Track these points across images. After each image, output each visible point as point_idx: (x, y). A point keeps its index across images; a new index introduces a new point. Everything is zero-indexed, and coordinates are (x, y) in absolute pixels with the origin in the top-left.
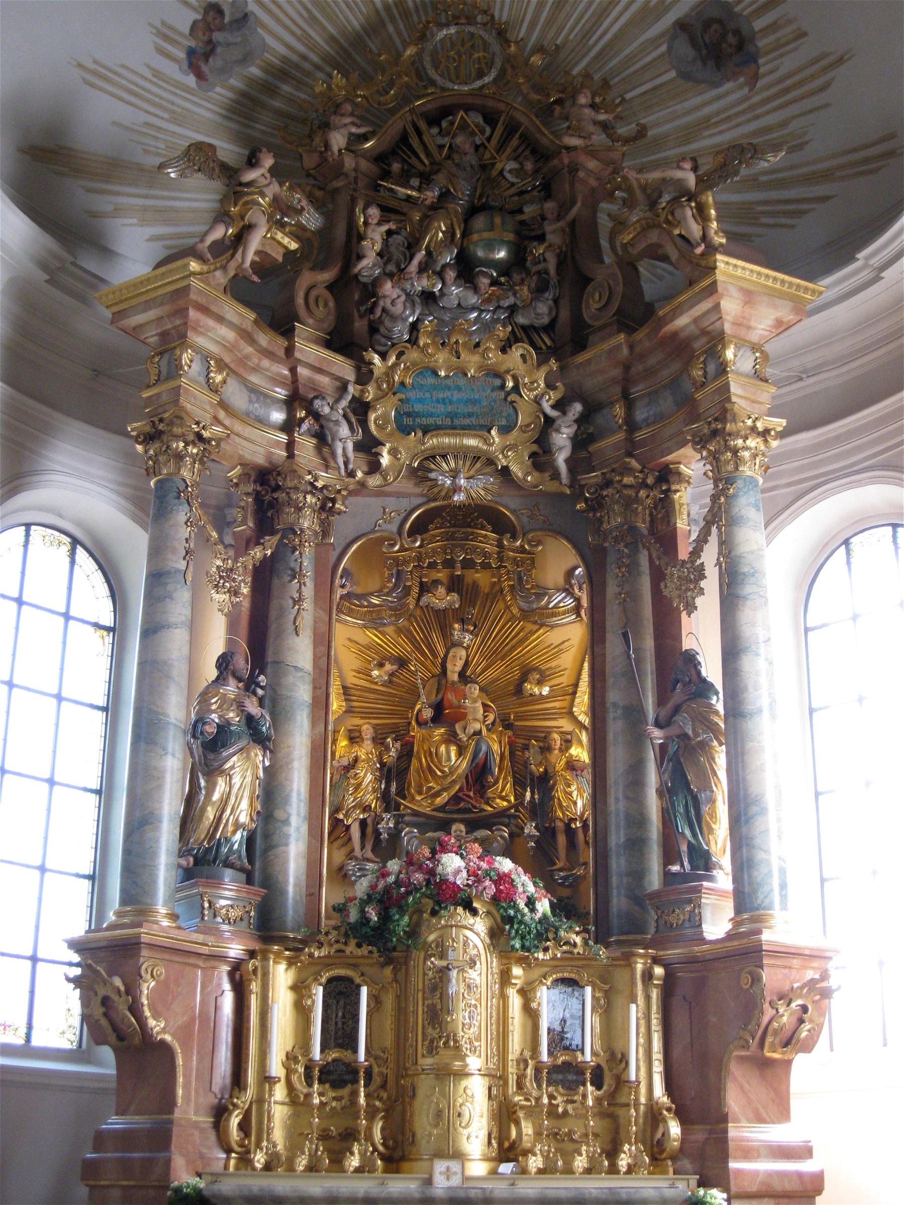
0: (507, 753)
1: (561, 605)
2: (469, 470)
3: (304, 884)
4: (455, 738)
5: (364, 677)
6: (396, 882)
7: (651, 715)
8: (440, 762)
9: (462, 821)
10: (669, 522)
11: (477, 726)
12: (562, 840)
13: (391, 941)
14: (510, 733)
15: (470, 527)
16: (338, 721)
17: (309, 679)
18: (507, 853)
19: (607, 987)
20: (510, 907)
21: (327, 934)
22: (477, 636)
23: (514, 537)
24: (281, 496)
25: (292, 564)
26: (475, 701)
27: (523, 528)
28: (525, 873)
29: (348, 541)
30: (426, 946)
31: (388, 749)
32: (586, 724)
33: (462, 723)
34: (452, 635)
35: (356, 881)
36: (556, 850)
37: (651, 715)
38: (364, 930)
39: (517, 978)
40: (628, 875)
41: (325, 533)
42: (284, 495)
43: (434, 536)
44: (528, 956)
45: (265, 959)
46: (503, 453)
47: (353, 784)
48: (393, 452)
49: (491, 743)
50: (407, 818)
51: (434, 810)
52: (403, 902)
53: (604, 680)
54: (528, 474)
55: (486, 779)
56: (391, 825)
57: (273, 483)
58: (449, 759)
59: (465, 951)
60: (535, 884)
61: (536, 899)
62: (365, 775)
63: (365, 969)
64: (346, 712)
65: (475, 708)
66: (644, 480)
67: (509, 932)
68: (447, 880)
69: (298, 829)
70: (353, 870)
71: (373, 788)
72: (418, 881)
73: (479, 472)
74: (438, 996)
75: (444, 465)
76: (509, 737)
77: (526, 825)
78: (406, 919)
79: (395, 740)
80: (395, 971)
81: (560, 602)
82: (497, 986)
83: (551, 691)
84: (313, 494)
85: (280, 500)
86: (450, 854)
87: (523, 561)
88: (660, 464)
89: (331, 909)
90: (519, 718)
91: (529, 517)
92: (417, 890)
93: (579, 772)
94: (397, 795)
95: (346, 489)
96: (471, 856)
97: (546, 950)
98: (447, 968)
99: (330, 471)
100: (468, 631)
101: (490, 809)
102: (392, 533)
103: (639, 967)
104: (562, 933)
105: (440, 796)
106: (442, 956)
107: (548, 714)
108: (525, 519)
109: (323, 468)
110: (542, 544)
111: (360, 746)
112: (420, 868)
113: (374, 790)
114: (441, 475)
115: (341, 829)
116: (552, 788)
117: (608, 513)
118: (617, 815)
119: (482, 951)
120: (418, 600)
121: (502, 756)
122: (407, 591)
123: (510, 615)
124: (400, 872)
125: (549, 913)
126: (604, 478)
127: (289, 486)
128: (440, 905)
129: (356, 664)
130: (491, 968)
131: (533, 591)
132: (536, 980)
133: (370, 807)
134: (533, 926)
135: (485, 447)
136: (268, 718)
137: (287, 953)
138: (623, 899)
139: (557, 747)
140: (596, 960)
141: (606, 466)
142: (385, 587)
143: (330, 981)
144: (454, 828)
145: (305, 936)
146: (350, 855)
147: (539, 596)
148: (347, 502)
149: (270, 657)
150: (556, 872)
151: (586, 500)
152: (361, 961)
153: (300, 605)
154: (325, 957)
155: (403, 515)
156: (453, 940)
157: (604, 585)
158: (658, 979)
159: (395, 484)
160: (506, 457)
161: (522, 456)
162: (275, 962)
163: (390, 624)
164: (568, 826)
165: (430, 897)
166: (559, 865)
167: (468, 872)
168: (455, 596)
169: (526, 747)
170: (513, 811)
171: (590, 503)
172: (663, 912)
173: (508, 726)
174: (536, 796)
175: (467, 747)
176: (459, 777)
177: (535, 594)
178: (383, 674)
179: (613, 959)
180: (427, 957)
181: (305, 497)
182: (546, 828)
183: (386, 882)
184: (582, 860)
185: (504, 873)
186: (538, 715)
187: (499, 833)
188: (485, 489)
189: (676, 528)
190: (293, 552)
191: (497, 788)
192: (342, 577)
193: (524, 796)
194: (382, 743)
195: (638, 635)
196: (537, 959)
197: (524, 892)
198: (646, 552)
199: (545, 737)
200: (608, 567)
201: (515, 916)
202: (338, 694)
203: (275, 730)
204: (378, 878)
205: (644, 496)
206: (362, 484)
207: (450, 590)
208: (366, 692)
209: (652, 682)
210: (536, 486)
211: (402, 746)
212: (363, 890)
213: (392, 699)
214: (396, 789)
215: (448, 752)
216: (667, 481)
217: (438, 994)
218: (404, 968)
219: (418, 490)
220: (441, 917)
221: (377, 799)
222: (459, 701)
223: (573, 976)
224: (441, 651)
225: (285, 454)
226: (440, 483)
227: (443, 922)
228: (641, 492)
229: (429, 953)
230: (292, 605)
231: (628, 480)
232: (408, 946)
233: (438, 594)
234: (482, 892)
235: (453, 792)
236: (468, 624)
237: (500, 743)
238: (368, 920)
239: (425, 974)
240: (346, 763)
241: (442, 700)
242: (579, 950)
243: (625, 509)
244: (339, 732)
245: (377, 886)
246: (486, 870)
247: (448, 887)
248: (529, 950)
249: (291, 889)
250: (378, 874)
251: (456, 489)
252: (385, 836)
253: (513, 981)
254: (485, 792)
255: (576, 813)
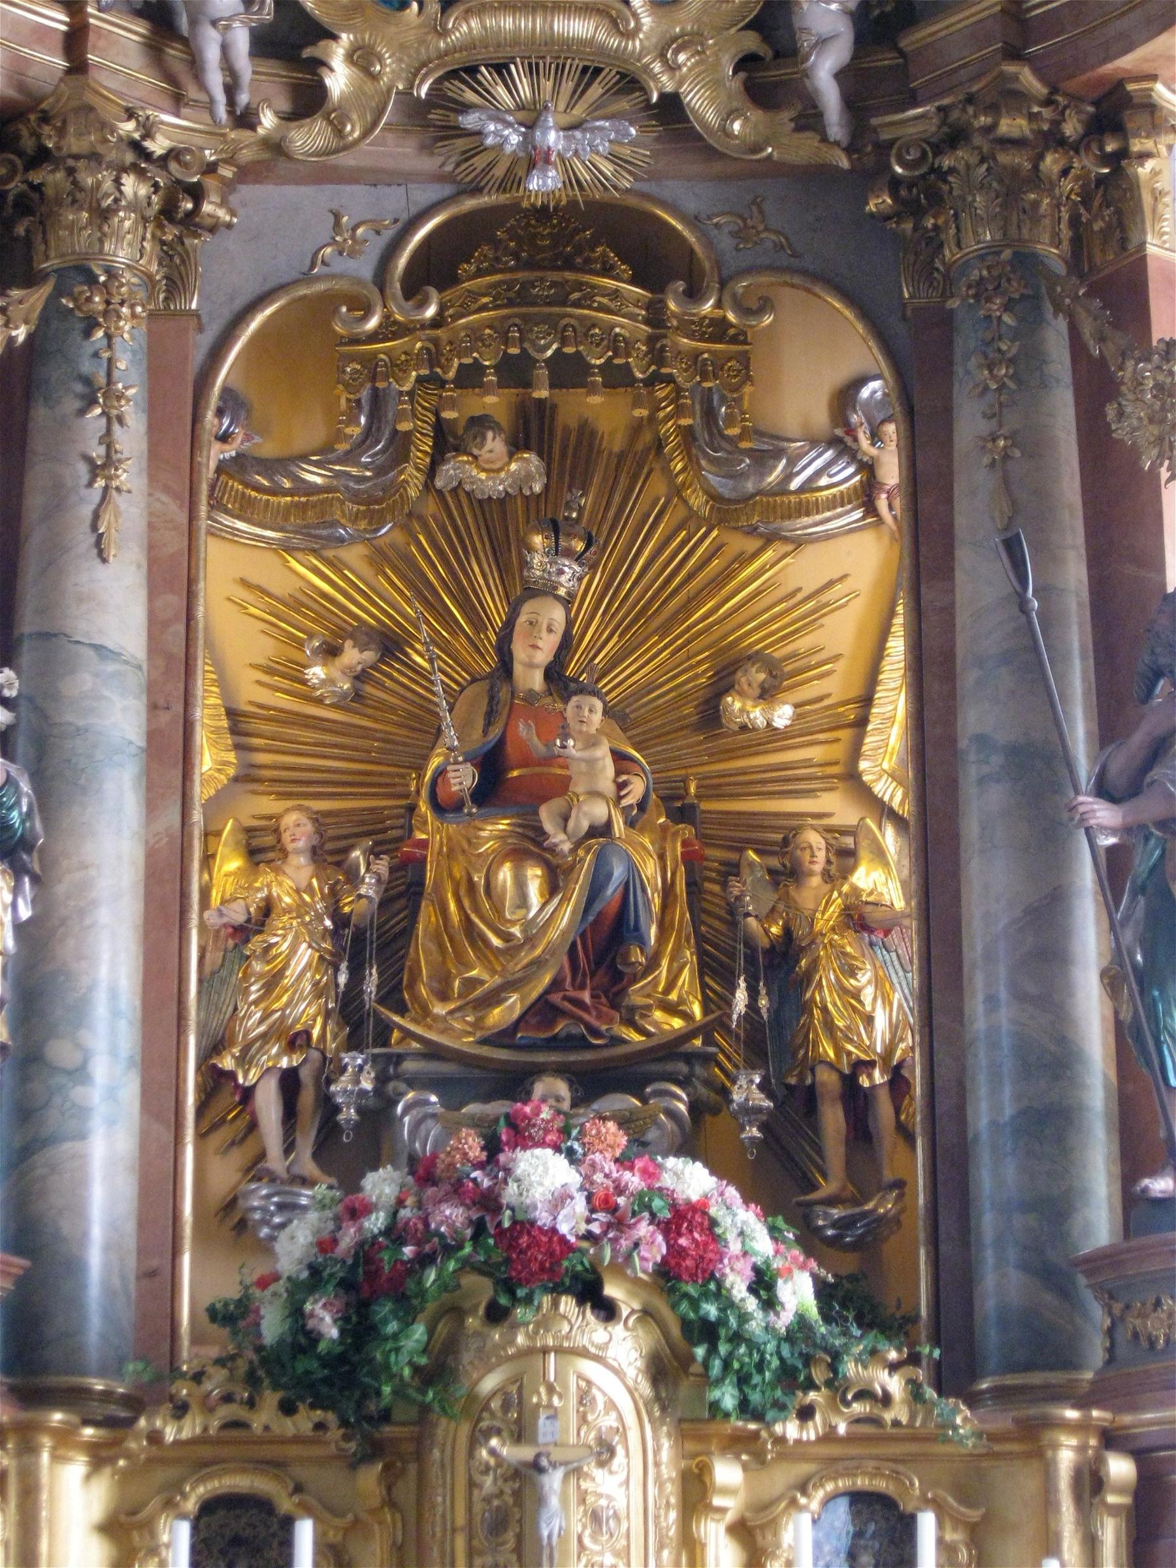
0: (681, 886)
1: (824, 481)
2: (570, 106)
3: (131, 1243)
4: (539, 844)
5: (286, 684)
6: (388, 1231)
7: (1084, 768)
8: (499, 910)
9: (560, 1070)
10: (1124, 242)
11: (599, 811)
12: (833, 1119)
13: (378, 1393)
14: (687, 831)
15: (569, 265)
16: (215, 805)
17: (136, 680)
18: (688, 1148)
19: (974, 1515)
20: (706, 1295)
21: (198, 1377)
22: (593, 567)
23: (694, 294)
24: (52, 178)
25: (86, 367)
26: (591, 742)
27: (718, 264)
28: (747, 1200)
29: (239, 303)
30: (475, 1407)
31: (353, 878)
32: (895, 804)
33: (557, 804)
34: (525, 564)
35: (272, 1238)
36: (820, 1151)
37: (1084, 768)
38: (302, 1365)
39: (726, 1491)
40: (1026, 1207)
41: (176, 284)
42: (60, 175)
43: (474, 295)
44: (756, 1435)
45: (28, 1449)
46: (662, 55)
47: (261, 976)
48: (361, 58)
49: (636, 858)
50: (409, 1066)
51: (484, 1042)
52: (410, 1285)
53: (949, 674)
54: (731, 114)
55: (627, 954)
56: (367, 1085)
57: (28, 144)
58: (523, 901)
59: (583, 1419)
60: (773, 1231)
61: (778, 1273)
62: (293, 949)
63: (301, 1473)
64: (236, 779)
65: (592, 762)
66: (1056, 124)
67: (706, 1364)
68: (532, 1223)
69: (111, 1094)
70: (264, 1209)
71: (316, 984)
72: (451, 1226)
73: (596, 109)
74: (511, 1544)
75: (501, 91)
76: (685, 844)
77: (734, 1081)
78: (419, 1332)
79: (374, 853)
80: (390, 1478)
81: (818, 474)
82: (673, 1515)
83: (797, 717)
84: (141, 174)
85: (49, 192)
86: (538, 1151)
87: (716, 367)
88: (1101, 80)
89: (204, 1318)
90: (712, 790)
91: (734, 234)
92: (449, 1250)
93: (877, 937)
94: (381, 1001)
95: (229, 161)
96: (598, 1157)
97: (806, 1414)
98: (536, 1467)
99: (185, 111)
100: (569, 553)
101: (636, 1037)
102: (359, 282)
103: (1066, 1457)
104: (850, 1368)
105: (500, 1002)
106: (521, 1433)
107: (788, 780)
108: (726, 243)
109: (167, 103)
110: (773, 309)
111: (278, 871)
112: (457, 1190)
113: (319, 991)
114: (492, 118)
115: (227, 1099)
116: (807, 977)
117: (956, 215)
118: (994, 1045)
119: (631, 1419)
120: (431, 472)
121: (668, 892)
122: (401, 446)
123: (682, 513)
124: (400, 1203)
125: (813, 1312)
126: (944, 123)
127: (75, 149)
128: (512, 1293)
129: (264, 648)
130: (657, 1465)
131: (744, 445)
132: (778, 1499)
133: (307, 1033)
134: (771, 1347)
135: (614, 42)
136: (25, 787)
137: (89, 1432)
138: (1015, 1277)
139: (818, 867)
140: (947, 1440)
141: (948, 91)
142: (339, 436)
143: (208, 1507)
144: (539, 1089)
145: (139, 1386)
146: (255, 1169)
147: (763, 459)
148: (233, 199)
149: (28, 622)
150: (819, 1209)
151: (895, 184)
152: (293, 1451)
153: (109, 478)
154: (192, 1442)
155: (388, 235)
156: (551, 1390)
157: (945, 417)
158: (1120, 1490)
159: (364, 146)
160: (672, 68)
161: (717, 64)
162: (56, 1458)
163: (353, 540)
164: (849, 1082)
165: (483, 1270)
166: (827, 1188)
167: (589, 1199)
168: (531, 461)
169: (732, 869)
170: (698, 1042)
171: (903, 193)
172: (1128, 1307)
173: (682, 813)
174: (763, 1002)
175: (571, 868)
176: (551, 950)
177: (750, 452)
178: (336, 674)
179: (993, 1438)
180: (478, 1437)
181: (118, 182)
182: (789, 1087)
183: (360, 1229)
184: (888, 1176)
185: (688, 1203)
186: (764, 782)
187: (665, 1102)
188: (613, 158)
189: (1143, 258)
190: (88, 333)
191: (655, 981)
192: (220, 413)
193: (729, 1004)
194: (338, 864)
195: (1048, 553)
196: (781, 1440)
197: (745, 1254)
198: (1062, 324)
199: (786, 842)
200: (959, 370)
201: (722, 1322)
202: (217, 731)
203: (45, 820)
204: (338, 1220)
205: (1056, 169)
206: (276, 147)
207: (517, 445)
208: (293, 724)
209: (1085, 679)
210: (757, 148)
211: (392, 870)
212: (298, 1253)
213: (366, 743)
214: (379, 987)
215: (520, 884)
216: (1119, 129)
217: (510, 1536)
218: (412, 1468)
219: (428, 164)
220: (515, 1327)
221: (327, 1015)
222: (549, 745)
223: (881, 1485)
224: (496, 611)
225: (60, 63)
226: (489, 141)
227: (520, 1339)
228: (1049, 159)
229: (484, 1424)
230: (85, 478)
231: (1012, 125)
232: (425, 1409)
233: (484, 453)
234: (628, 1257)
235: (536, 990)
236: (569, 535)
237: (662, 857)
238: (314, 1338)
239: (472, 1485)
240: (240, 918)
241: (501, 743)
242: (899, 1412)
243: (1005, 206)
244: (218, 834)
245: (335, 1242)
246: (640, 1195)
247: (534, 1243)
248: (758, 1416)
249: (95, 1259)
250: (340, 1208)
251: (534, 158)
252: (349, 1114)
253: (717, 1501)
254: (623, 992)
255: (871, 1048)
